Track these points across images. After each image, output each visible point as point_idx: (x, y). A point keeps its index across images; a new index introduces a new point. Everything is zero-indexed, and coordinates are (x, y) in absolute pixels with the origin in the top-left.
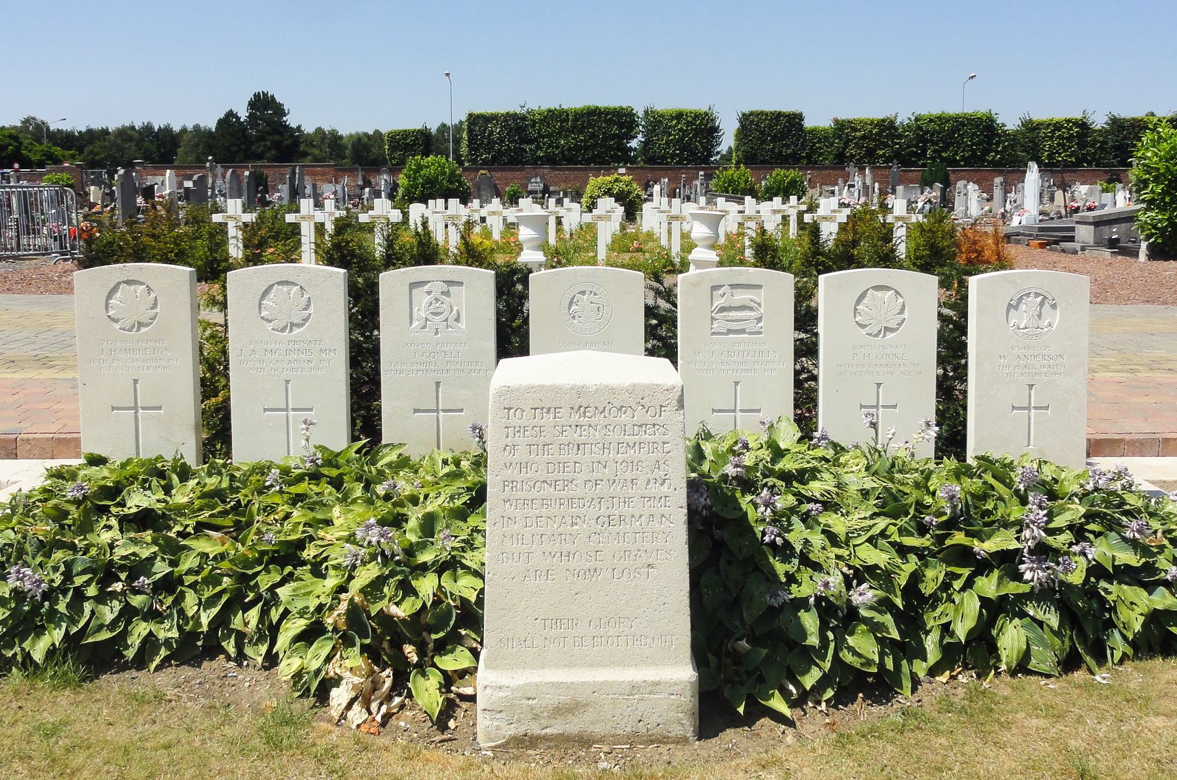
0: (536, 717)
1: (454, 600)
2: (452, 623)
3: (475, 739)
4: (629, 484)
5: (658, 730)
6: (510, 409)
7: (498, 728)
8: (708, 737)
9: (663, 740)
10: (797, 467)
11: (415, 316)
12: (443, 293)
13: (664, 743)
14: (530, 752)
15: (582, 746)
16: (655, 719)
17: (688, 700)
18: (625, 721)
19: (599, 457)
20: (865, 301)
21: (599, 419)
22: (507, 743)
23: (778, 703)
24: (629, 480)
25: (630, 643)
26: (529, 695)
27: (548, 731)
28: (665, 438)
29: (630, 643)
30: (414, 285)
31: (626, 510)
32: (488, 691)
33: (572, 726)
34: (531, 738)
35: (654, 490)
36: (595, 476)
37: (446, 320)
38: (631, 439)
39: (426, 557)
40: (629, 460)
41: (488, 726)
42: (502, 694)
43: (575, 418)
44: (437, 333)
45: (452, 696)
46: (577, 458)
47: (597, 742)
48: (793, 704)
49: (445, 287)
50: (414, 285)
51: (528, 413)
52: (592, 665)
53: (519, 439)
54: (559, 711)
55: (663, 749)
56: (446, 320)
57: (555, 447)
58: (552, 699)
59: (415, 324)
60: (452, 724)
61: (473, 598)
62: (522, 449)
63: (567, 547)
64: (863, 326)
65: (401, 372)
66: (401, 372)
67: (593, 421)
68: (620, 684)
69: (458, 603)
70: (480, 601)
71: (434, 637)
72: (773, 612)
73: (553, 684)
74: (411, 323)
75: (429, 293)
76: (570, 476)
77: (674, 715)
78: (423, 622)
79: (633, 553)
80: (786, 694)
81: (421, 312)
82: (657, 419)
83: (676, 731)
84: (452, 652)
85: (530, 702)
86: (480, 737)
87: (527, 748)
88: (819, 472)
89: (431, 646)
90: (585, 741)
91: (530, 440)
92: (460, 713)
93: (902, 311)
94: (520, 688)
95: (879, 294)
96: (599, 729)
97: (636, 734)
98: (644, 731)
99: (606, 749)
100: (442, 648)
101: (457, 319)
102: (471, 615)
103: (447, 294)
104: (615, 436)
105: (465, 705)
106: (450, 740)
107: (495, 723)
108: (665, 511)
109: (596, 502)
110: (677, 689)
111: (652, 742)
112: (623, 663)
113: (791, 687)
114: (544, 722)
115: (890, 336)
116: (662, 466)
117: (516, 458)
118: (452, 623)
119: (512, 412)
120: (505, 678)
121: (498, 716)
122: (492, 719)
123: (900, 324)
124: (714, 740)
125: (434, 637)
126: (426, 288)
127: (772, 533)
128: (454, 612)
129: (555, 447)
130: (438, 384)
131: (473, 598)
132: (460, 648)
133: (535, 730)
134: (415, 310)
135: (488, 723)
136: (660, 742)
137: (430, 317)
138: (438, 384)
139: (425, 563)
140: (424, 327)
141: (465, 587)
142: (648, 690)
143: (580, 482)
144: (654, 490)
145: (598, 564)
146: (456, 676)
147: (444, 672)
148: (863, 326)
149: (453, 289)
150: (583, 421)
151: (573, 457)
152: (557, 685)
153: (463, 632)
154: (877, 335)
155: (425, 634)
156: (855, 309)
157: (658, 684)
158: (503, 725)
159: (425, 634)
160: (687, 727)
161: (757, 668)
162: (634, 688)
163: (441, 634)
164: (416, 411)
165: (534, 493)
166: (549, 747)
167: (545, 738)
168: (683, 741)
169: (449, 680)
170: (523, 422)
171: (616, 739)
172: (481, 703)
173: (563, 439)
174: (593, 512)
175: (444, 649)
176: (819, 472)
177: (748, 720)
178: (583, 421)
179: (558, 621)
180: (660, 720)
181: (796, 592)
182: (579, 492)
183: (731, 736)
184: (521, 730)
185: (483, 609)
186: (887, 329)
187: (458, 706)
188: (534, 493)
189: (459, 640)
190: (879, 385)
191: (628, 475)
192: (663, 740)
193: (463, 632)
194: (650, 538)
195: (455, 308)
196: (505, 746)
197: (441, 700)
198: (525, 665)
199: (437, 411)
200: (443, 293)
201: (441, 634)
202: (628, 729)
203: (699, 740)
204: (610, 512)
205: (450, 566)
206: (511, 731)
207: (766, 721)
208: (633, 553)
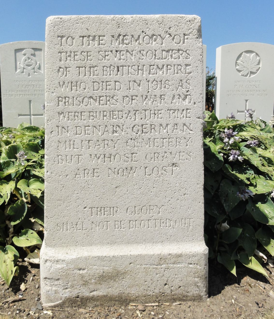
0: (86, 284)
1: (26, 198)
2: (25, 214)
3: (39, 299)
4: (158, 99)
5: (179, 291)
6: (62, 37)
7: (56, 292)
8: (215, 295)
9: (183, 298)
10: (233, 124)
11: (18, 67)
12: (32, 55)
13: (184, 300)
14: (82, 310)
15: (122, 304)
16: (177, 283)
17: (202, 268)
18: (154, 284)
19: (134, 77)
20: (241, 58)
21: (135, 45)
22: (64, 303)
23: (254, 265)
24: (158, 96)
25: (158, 225)
26: (80, 266)
27: (95, 293)
28: (187, 61)
29: (158, 225)
30: (17, 51)
31: (156, 120)
32: (48, 264)
33: (113, 289)
34: (82, 299)
35: (178, 103)
36: (132, 92)
37: (34, 69)
38: (160, 62)
39: (11, 171)
40: (159, 80)
41: (48, 289)
42: (59, 266)
43: (116, 45)
44: (29, 75)
45: (26, 264)
46: (117, 78)
47: (133, 301)
48: (264, 265)
49: (33, 52)
50: (17, 51)
51: (77, 41)
52: (129, 242)
53: (70, 62)
54: (103, 278)
55: (185, 306)
56: (34, 69)
57: (99, 68)
58: (98, 269)
59: (18, 71)
60: (23, 287)
61: (39, 195)
62: (73, 70)
63: (109, 150)
64: (239, 71)
65: (12, 95)
66: (12, 95)
67: (130, 47)
68: (151, 256)
69: (29, 199)
70: (42, 197)
71: (13, 224)
72: (243, 204)
73: (99, 258)
74: (16, 70)
75: (25, 55)
76: (112, 92)
77: (191, 279)
78: (6, 214)
79: (161, 155)
80: (260, 260)
81: (21, 65)
82: (182, 46)
83: (193, 291)
84: (25, 233)
85: (81, 272)
86: (43, 299)
87: (79, 307)
88: (245, 127)
89: (11, 230)
90: (123, 301)
91: (79, 63)
92: (30, 277)
93: (259, 63)
94: (73, 261)
95: (248, 55)
96: (134, 292)
97: (162, 294)
98: (169, 292)
99: (141, 307)
100: (19, 231)
101: (39, 68)
102: (36, 207)
103: (34, 55)
104: (147, 60)
105: (34, 271)
106: (20, 300)
107: (54, 288)
108: (187, 121)
109: (132, 114)
110: (195, 259)
111: (175, 300)
112: (153, 241)
113: (261, 254)
114: (92, 287)
115: (253, 76)
116: (185, 84)
117: (69, 77)
118: (25, 214)
119: (64, 39)
120: (61, 255)
121: (56, 283)
122: (51, 286)
123: (258, 70)
124: (219, 296)
125: (13, 224)
126: (23, 52)
127: (235, 154)
128: (26, 206)
129: (99, 68)
130: (30, 101)
131: (39, 195)
132: (31, 231)
133: (85, 293)
134: (18, 63)
135: (48, 288)
136: (180, 300)
137: (26, 67)
138: (30, 101)
139: (10, 175)
140: (23, 72)
141: (35, 189)
142: (172, 261)
143: (120, 97)
144: (178, 103)
145: (134, 164)
146: (28, 251)
147: (19, 249)
148: (239, 71)
149: (37, 53)
150: (122, 47)
151: (114, 77)
152: (101, 259)
153: (33, 220)
154: (246, 76)
155: (7, 222)
156: (236, 63)
157: (180, 256)
158: (60, 289)
159: (7, 222)
160: (201, 288)
161: (237, 241)
162: (162, 259)
163: (18, 222)
164: (19, 115)
165: (82, 107)
166: (96, 306)
167: (93, 299)
168: (199, 298)
169: (23, 253)
170: (74, 48)
171: (147, 299)
172: (43, 272)
173: (106, 62)
174: (129, 122)
175: (20, 232)
176: (245, 127)
177: (237, 280)
178: (122, 47)
179: (102, 209)
180: (181, 284)
181: (253, 191)
182: (119, 106)
183: (229, 291)
184: (75, 293)
185: (43, 203)
186: (252, 73)
187: (30, 272)
188: (82, 107)
189: (31, 226)
190: (247, 101)
191: (158, 92)
192: (183, 298)
193: (33, 220)
194: (174, 142)
195: (38, 63)
196: (61, 306)
197: (14, 269)
198: (76, 243)
199: (30, 115)
200: (32, 55)
201: (18, 222)
202: (157, 291)
203: (209, 297)
204: (143, 122)
205: (26, 175)
206: (67, 294)
207: (247, 279)
208: (161, 155)
